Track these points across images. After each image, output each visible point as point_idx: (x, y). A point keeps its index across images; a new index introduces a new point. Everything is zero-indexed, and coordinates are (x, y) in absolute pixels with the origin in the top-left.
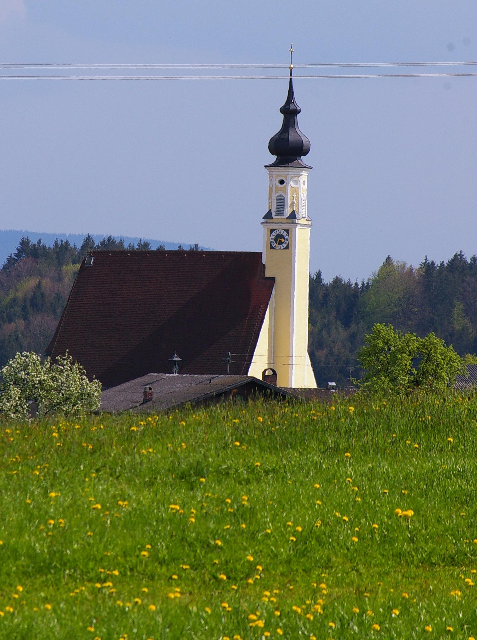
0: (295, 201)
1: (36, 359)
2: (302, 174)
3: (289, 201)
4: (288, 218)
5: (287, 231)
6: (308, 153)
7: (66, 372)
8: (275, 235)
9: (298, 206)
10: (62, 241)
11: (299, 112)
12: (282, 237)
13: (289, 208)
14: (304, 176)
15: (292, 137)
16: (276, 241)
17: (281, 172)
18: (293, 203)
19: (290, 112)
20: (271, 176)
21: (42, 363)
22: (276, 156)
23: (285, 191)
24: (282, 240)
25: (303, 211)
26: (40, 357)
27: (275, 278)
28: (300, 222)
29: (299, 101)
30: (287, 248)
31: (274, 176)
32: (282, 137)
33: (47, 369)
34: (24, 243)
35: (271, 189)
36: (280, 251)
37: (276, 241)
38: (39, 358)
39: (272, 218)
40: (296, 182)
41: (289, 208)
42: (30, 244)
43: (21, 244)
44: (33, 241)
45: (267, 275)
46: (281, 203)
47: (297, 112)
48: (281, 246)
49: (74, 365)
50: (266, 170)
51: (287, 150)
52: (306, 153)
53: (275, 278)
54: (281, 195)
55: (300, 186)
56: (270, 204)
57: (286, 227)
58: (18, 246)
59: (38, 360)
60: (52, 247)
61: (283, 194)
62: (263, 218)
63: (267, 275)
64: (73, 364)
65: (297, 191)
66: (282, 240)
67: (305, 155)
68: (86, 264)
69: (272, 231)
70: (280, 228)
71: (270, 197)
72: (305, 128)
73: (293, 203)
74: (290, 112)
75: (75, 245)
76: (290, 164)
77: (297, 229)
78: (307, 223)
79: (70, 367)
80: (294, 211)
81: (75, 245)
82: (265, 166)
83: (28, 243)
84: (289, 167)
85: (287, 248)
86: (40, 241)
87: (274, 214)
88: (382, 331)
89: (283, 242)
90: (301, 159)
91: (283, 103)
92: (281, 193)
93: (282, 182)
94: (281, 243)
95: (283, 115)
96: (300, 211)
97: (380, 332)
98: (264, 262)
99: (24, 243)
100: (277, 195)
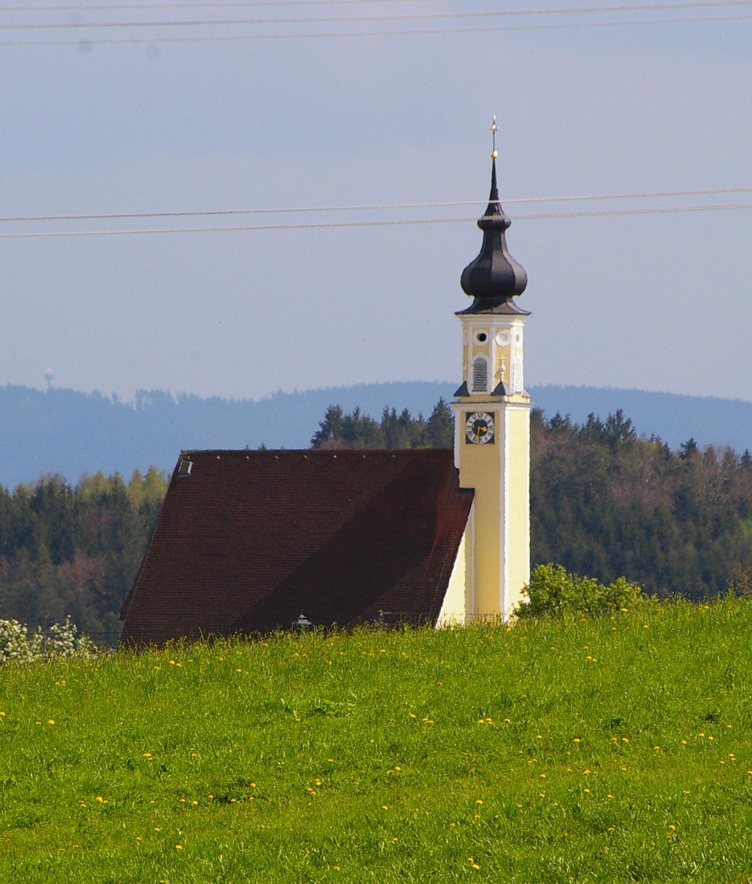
0: (503, 367)
1: (19, 631)
2: (513, 324)
3: (493, 369)
4: (492, 394)
5: (492, 415)
6: (523, 290)
7: (67, 651)
8: (473, 421)
9: (508, 375)
10: (394, 411)
11: (508, 226)
12: (483, 423)
13: (494, 379)
14: (517, 326)
15: (497, 265)
16: (475, 430)
17: (480, 322)
18: (500, 371)
19: (493, 229)
20: (465, 328)
21: (29, 636)
22: (472, 298)
23: (488, 351)
24: (484, 429)
25: (516, 383)
26: (26, 627)
27: (473, 490)
28: (512, 400)
29: (508, 208)
30: (492, 441)
31: (471, 329)
32: (481, 266)
33: (38, 645)
34: (333, 415)
35: (466, 348)
36: (481, 448)
37: (475, 430)
38: (25, 629)
39: (468, 395)
40: (506, 337)
41: (494, 379)
42: (342, 417)
43: (327, 416)
44: (347, 411)
45: (463, 484)
46: (481, 371)
47: (503, 226)
48: (483, 438)
49: (80, 638)
50: (457, 319)
51: (491, 287)
52: (520, 290)
53: (473, 490)
54: (480, 359)
55: (512, 345)
56: (466, 372)
57: (491, 408)
58: (323, 419)
59: (22, 632)
60: (427, 416)
61: (485, 357)
62: (455, 395)
63: (463, 484)
64: (77, 636)
65: (506, 351)
66: (484, 429)
67: (519, 293)
68: (181, 473)
69: (469, 415)
70: (481, 410)
71: (465, 362)
72: (517, 250)
73: (500, 371)
74: (493, 229)
75: (421, 417)
76: (495, 310)
77: (507, 412)
78: (524, 401)
79: (73, 642)
80: (501, 383)
81: (421, 417)
82: (457, 313)
83: (339, 413)
84: (492, 313)
85: (492, 441)
86: (358, 411)
87: (470, 388)
88: (547, 577)
89: (485, 433)
90: (512, 302)
91: (480, 212)
92: (481, 355)
93: (482, 337)
94: (482, 433)
95: (482, 232)
96: (511, 383)
97: (544, 579)
98: (457, 465)
99: (333, 415)
100: (476, 357)
